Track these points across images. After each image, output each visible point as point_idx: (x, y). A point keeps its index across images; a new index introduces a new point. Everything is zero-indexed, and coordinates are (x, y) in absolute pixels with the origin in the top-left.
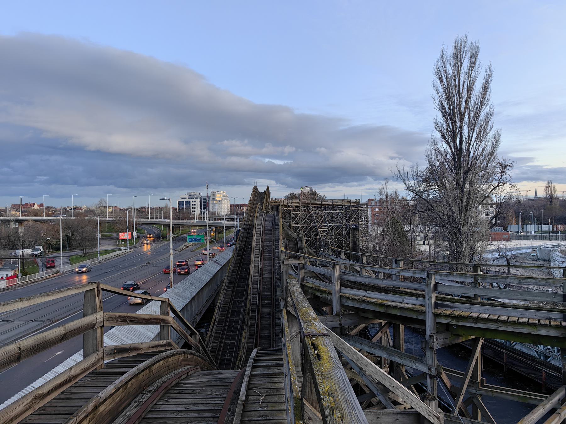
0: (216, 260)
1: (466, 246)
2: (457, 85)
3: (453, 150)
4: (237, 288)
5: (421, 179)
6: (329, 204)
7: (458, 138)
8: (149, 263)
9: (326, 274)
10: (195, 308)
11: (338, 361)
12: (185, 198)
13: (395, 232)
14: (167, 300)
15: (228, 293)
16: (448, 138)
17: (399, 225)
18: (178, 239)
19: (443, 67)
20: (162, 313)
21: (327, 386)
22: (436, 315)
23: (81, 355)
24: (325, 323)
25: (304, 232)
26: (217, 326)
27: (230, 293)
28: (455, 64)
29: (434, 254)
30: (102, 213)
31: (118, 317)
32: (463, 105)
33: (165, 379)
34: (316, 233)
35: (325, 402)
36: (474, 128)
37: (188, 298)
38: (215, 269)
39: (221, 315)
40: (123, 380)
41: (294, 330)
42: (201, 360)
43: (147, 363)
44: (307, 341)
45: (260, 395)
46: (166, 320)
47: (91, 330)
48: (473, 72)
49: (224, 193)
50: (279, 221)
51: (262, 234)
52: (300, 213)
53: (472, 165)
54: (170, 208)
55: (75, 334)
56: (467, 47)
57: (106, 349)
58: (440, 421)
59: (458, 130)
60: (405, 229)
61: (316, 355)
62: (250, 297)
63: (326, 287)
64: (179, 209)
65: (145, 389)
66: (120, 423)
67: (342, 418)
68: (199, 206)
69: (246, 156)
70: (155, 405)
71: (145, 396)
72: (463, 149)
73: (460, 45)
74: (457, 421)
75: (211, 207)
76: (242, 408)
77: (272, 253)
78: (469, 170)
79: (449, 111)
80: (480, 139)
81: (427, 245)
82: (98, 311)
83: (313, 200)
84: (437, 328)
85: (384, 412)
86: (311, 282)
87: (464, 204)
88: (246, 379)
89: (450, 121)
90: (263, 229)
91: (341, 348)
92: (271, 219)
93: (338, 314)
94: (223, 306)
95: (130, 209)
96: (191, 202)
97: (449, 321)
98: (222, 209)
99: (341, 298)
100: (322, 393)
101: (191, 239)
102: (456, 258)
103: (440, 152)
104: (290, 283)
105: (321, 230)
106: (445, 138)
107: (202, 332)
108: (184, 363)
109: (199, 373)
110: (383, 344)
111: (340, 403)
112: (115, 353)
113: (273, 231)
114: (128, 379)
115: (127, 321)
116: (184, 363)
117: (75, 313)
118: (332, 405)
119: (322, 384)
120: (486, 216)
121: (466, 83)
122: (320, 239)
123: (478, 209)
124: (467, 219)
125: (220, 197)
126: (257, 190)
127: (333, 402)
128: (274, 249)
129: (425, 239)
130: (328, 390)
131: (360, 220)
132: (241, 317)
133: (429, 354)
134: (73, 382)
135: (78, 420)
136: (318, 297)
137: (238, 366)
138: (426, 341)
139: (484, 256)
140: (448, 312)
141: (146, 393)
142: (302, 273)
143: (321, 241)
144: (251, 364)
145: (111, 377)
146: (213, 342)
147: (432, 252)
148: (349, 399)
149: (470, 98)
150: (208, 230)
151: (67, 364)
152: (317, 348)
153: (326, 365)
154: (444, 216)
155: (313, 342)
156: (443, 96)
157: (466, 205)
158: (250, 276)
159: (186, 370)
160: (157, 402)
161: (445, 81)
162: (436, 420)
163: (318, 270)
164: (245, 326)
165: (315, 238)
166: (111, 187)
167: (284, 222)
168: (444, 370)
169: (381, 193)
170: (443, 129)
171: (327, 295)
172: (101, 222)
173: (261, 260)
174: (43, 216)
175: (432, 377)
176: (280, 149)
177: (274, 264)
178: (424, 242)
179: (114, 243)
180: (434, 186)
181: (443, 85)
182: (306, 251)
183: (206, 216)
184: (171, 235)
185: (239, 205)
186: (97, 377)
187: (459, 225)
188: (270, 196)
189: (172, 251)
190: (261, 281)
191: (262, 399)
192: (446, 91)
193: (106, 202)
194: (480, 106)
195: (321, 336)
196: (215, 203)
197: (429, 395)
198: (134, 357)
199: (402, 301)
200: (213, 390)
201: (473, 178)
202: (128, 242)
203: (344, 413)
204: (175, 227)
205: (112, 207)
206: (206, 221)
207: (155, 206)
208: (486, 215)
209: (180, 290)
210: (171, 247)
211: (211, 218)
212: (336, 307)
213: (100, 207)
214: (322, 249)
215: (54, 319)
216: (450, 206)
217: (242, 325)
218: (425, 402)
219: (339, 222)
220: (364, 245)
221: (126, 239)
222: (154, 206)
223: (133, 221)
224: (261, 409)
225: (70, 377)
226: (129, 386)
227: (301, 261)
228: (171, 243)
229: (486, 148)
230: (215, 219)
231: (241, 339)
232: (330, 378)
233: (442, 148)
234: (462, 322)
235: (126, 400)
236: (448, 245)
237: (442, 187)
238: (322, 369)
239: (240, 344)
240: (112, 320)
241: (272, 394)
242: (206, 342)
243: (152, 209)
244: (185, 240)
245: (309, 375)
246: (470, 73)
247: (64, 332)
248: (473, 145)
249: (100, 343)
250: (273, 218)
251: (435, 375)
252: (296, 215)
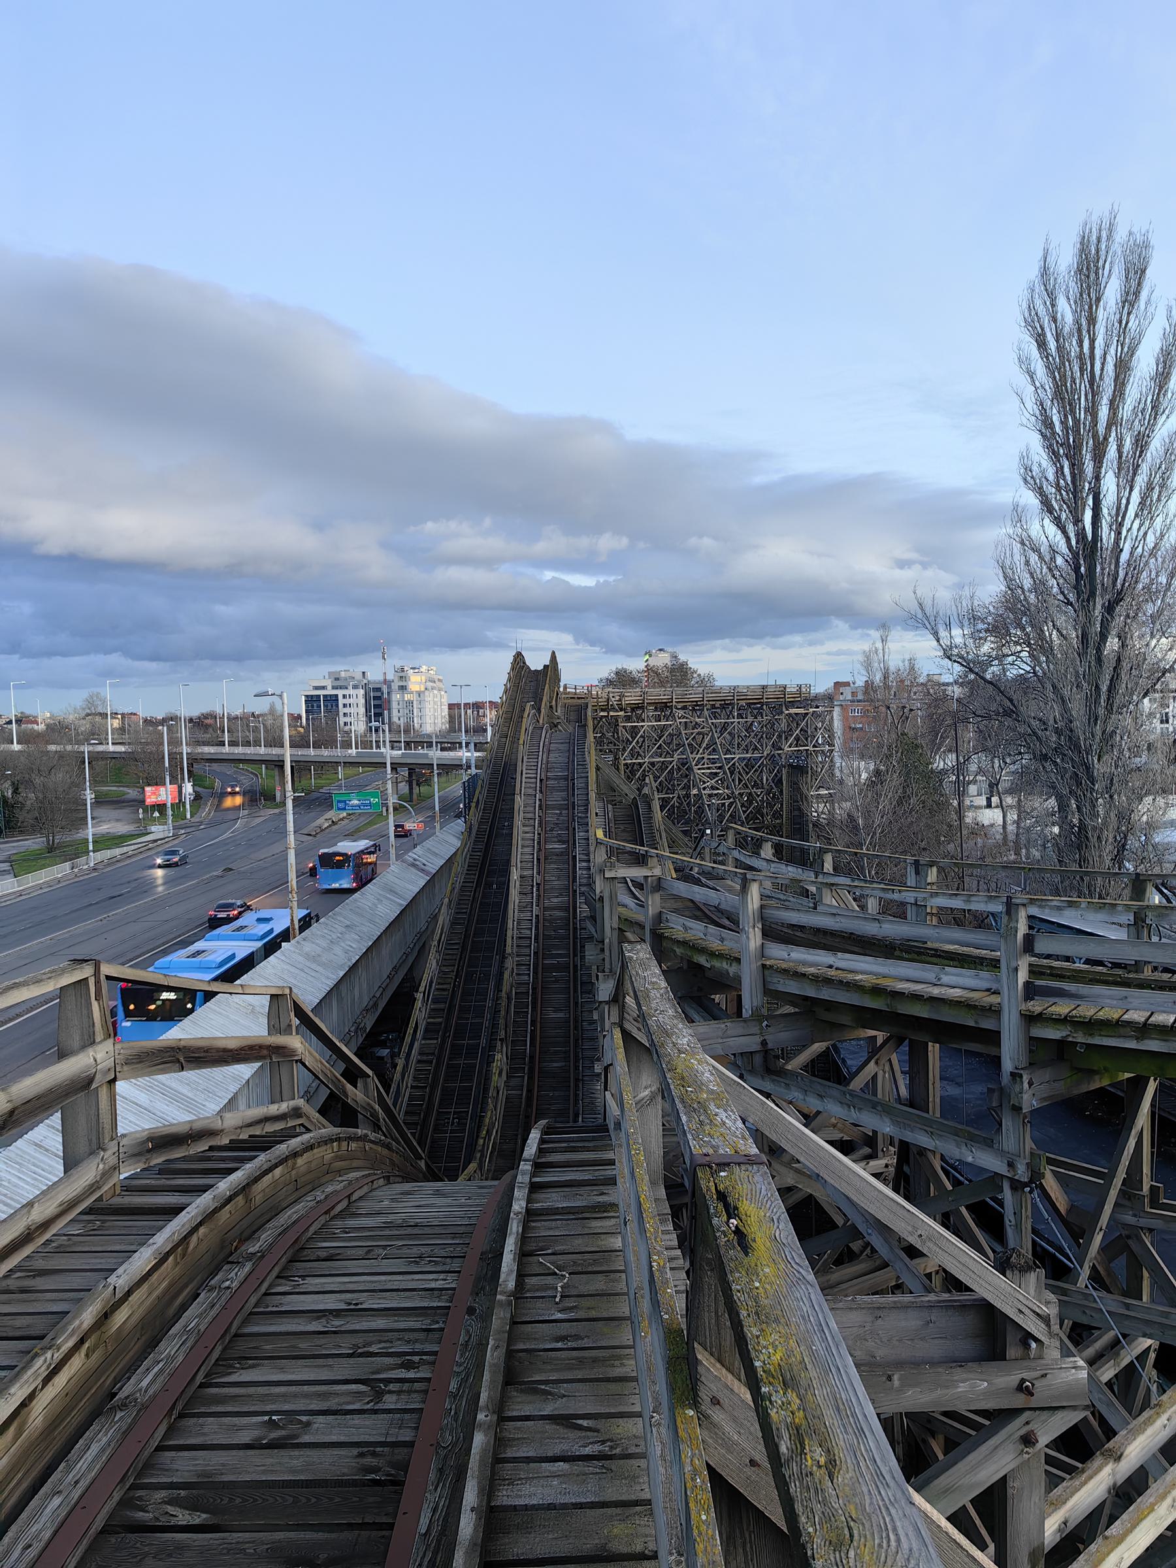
0: (415, 860)
1: (1107, 813)
2: (1087, 356)
3: (1074, 542)
4: (474, 937)
5: (981, 626)
7: (1087, 507)
8: (231, 870)
9: (722, 907)
10: (362, 993)
11: (800, 1256)
12: (323, 688)
13: (908, 773)
14: (287, 991)
15: (447, 957)
16: (1061, 510)
17: (921, 754)
18: (312, 802)
19: (1048, 303)
20: (273, 1029)
21: (775, 1348)
22: (1030, 1019)
23: (53, 1128)
24: (721, 1041)
25: (656, 778)
26: (423, 1042)
27: (455, 952)
28: (1081, 295)
29: (1017, 835)
30: (96, 734)
31: (154, 1053)
32: (1104, 412)
33: (289, 1217)
34: (689, 781)
35: (775, 1410)
36: (1133, 479)
37: (341, 967)
38: (413, 883)
39: (433, 1013)
40: (174, 1233)
41: (644, 1084)
42: (385, 1152)
43: (237, 1177)
44: (703, 1183)
45: (555, 1274)
46: (284, 1048)
47: (82, 1094)
48: (1132, 317)
49: (431, 672)
51: (541, 788)
52: (642, 726)
53: (1127, 584)
54: (282, 715)
55: (37, 1109)
56: (1116, 247)
57: (124, 1142)
58: (1048, 1325)
59: (1087, 485)
60: (936, 765)
61: (734, 1232)
62: (509, 963)
63: (722, 940)
64: (307, 719)
65: (236, 1249)
66: (172, 1353)
67: (831, 1466)
68: (362, 710)
69: (489, 562)
70: (266, 1294)
71: (236, 1270)
72: (1101, 540)
73: (1095, 241)
74: (1086, 1303)
75: (395, 713)
76: (509, 1316)
77: (570, 841)
78: (1119, 598)
79: (1062, 431)
80: (1151, 509)
81: (997, 807)
82: (98, 1039)
83: (679, 690)
84: (1031, 1051)
85: (895, 1302)
86: (681, 927)
87: (1103, 697)
88: (515, 1227)
89: (1065, 459)
91: (776, 1132)
92: (563, 747)
93: (757, 1017)
94: (438, 989)
95: (172, 719)
96: (340, 697)
97: (1064, 1034)
98: (428, 718)
99: (766, 972)
100: (764, 1376)
101: (345, 801)
102: (1079, 848)
103: (1036, 550)
104: (631, 958)
106: (1050, 510)
107: (382, 1058)
108: (339, 1164)
109: (381, 1193)
110: (880, 1095)
111: (819, 1413)
112: (149, 1151)
113: (570, 780)
114: (188, 1228)
115: (178, 1061)
116: (339, 1164)
118: (797, 1420)
119: (762, 1342)
120: (1162, 726)
121: (1112, 351)
122: (699, 796)
123: (1140, 706)
124: (1111, 737)
126: (524, 663)
127: (799, 1409)
128: (574, 829)
129: (992, 792)
130: (779, 1365)
131: (811, 742)
132: (487, 1015)
133: (1010, 1123)
134: (37, 1240)
135: (56, 1356)
136: (700, 967)
137: (482, 1151)
138: (1001, 1089)
139: (1157, 840)
140: (1062, 1008)
141: (239, 1263)
142: (654, 903)
144: (527, 1179)
145: (142, 1223)
146: (412, 1087)
147: (1011, 828)
148: (843, 1396)
149: (1122, 394)
150: (389, 777)
151: (17, 1155)
152: (736, 1208)
153: (767, 1270)
154: (1046, 729)
155: (721, 1187)
156: (1047, 387)
157: (1108, 699)
158: (511, 906)
159: (345, 1187)
160: (271, 1286)
161: (1052, 345)
162: (1039, 1323)
163: (698, 893)
164: (499, 1043)
165: (688, 796)
166: (115, 659)
167: (601, 750)
168: (1050, 1161)
169: (868, 665)
170: (1045, 483)
171: (725, 963)
172: (95, 757)
173: (538, 860)
175: (1016, 1186)
176: (584, 542)
177: (575, 872)
178: (989, 800)
179: (132, 816)
180: (1016, 643)
181: (1047, 358)
182: (664, 834)
183: (384, 737)
184: (290, 794)
185: (473, 704)
186: (103, 1221)
187: (1087, 754)
188: (559, 681)
189: (291, 838)
190: (541, 918)
191: (562, 1287)
192: (1056, 374)
193: (104, 701)
194: (1150, 415)
195: (743, 1167)
197: (1019, 1256)
198: (201, 1158)
199: (934, 981)
200: (423, 1250)
201: (1129, 621)
202: (170, 812)
203: (836, 1452)
204: (300, 768)
205: (123, 715)
206: (383, 750)
207: (241, 711)
208: (1162, 722)
209: (317, 945)
210: (291, 826)
211: (396, 742)
212: (751, 997)
213: (88, 715)
214: (708, 831)
216: (1063, 701)
217: (491, 1040)
218: (1007, 1275)
219: (754, 750)
220: (822, 813)
221: (165, 805)
222: (238, 712)
223: (182, 753)
224: (559, 1316)
225: (28, 1229)
226: (192, 1246)
227: (651, 868)
228: (290, 818)
229: (1166, 537)
230: (408, 744)
231: (488, 1079)
232: (782, 1320)
233: (1043, 538)
234: (1100, 1035)
235: (186, 1286)
236: (1056, 809)
237: (1041, 647)
238: (757, 1284)
239: (486, 1090)
240: (140, 1062)
241: (590, 1269)
242: (394, 1087)
243: (233, 719)
244: (326, 802)
245: (710, 1280)
246: (1124, 322)
247: (9, 1107)
248: (1130, 529)
249: (107, 1127)
250: (570, 742)
251: (1026, 1180)
252: (634, 731)
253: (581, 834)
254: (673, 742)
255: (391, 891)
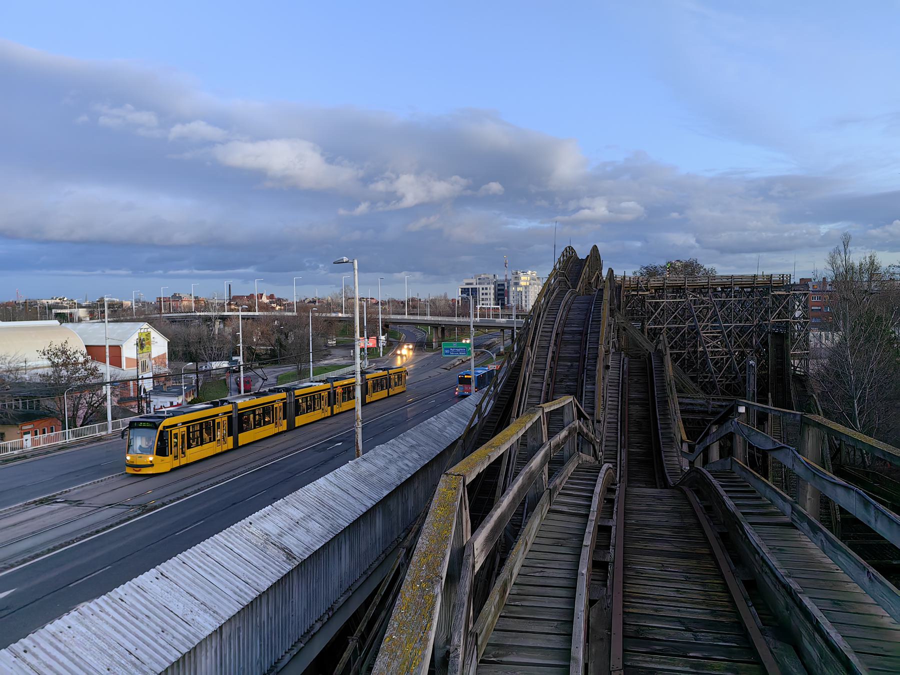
6: (724, 285)
34: (696, 342)
49: (534, 275)
50: (602, 310)
51: (556, 341)
68: (492, 297)
75: (511, 298)
90: (560, 329)
96: (481, 289)
101: (449, 349)
105: (707, 336)
117: (218, 483)
122: (704, 353)
125: (526, 281)
128: (583, 380)
143: (707, 358)
165: (695, 352)
174: (255, 311)
196: (518, 290)
214: (742, 410)
215: (150, 505)
219: (746, 322)
223: (379, 319)
230: (517, 317)
253: (588, 386)
254: (685, 314)
255: (463, 415)
